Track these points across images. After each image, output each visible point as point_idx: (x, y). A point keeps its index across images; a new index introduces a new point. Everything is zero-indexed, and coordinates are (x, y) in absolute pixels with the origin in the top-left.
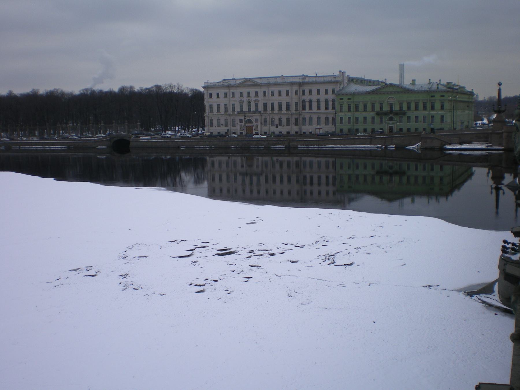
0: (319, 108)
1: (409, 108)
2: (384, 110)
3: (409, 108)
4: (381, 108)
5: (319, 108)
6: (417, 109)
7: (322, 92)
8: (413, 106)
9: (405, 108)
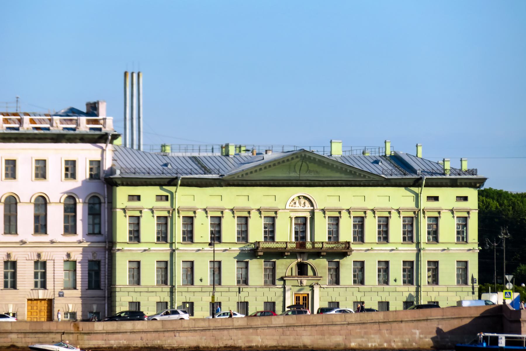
0: (41, 225)
5: (41, 225)
7: (25, 170)
9: (346, 233)
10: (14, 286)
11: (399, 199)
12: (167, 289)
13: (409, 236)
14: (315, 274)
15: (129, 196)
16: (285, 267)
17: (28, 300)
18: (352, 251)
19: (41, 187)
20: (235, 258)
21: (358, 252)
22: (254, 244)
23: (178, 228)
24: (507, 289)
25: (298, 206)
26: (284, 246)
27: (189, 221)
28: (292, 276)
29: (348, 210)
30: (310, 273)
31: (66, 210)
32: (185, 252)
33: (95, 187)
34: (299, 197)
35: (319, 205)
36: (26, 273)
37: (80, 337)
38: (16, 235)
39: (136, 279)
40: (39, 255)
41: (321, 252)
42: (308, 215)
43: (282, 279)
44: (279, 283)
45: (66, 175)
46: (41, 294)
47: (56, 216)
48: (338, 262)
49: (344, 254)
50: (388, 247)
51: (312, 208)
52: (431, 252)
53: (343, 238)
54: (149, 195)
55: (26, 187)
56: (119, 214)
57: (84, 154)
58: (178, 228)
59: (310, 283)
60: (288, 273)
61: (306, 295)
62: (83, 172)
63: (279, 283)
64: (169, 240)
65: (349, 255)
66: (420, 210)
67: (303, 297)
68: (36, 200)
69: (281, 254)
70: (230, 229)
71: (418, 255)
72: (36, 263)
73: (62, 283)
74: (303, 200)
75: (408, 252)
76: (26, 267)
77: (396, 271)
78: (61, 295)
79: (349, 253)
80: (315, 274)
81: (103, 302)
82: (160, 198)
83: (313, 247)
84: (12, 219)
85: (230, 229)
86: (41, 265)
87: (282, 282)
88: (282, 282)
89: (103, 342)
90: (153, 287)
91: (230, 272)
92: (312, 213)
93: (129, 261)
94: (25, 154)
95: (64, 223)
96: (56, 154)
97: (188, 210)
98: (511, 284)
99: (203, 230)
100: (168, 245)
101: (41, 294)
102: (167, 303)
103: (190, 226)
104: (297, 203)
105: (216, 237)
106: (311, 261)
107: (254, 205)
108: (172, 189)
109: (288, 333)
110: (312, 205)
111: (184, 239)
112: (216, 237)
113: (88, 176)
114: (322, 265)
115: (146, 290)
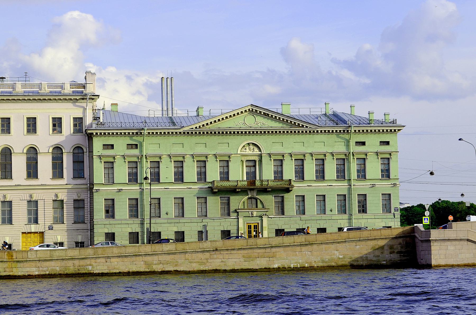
0: (32, 172)
1: (300, 174)
2: (232, 177)
3: (300, 174)
4: (225, 176)
5: (32, 172)
6: (321, 175)
7: (44, 125)
8: (310, 169)
9: (289, 172)
10: (10, 222)
11: (334, 145)
12: (138, 221)
13: (342, 174)
14: (263, 207)
15: (104, 145)
16: (237, 201)
17: (23, 233)
18: (293, 186)
19: (32, 140)
20: (195, 196)
21: (299, 188)
22: (211, 183)
23: (354, 167)
24: (425, 216)
25: (248, 152)
26: (236, 184)
27: (156, 165)
28: (244, 209)
29: (332, 153)
30: (260, 206)
31: (53, 159)
32: (360, 187)
33: (80, 140)
34: (248, 144)
35: (264, 151)
36: (20, 212)
37: (14, 265)
38: (11, 180)
39: (226, 212)
40: (31, 196)
41: (236, 189)
42: (257, 158)
43: (236, 211)
44: (234, 215)
45: (54, 130)
46: (33, 228)
47: (45, 164)
48: (283, 197)
49: (288, 190)
50: (389, 182)
51: (260, 153)
52: (360, 187)
53: (286, 177)
54: (121, 145)
55: (18, 140)
56: (96, 161)
57: (68, 113)
58: (354, 167)
59: (259, 214)
60: (241, 206)
61: (257, 224)
62: (68, 127)
63: (234, 215)
64: (346, 178)
65: (292, 190)
66: (350, 153)
67: (254, 226)
68: (28, 150)
69: (234, 191)
70: (191, 172)
71: (350, 190)
72: (29, 202)
73: (52, 218)
74: (252, 147)
75: (342, 187)
76: (20, 206)
77: (332, 203)
78: (51, 228)
79: (290, 189)
80: (263, 207)
81: (87, 234)
82: (131, 146)
83: (262, 185)
84: (8, 166)
85: (191, 172)
86: (33, 205)
87: (236, 214)
88: (236, 214)
89: (34, 269)
90: (126, 219)
91: (192, 206)
92: (261, 156)
93: (197, 198)
94: (18, 113)
95: (53, 169)
96: (44, 113)
97: (155, 156)
98: (428, 212)
99: (167, 172)
100: (346, 181)
101: (33, 228)
102: (138, 233)
103: (387, 166)
104: (247, 148)
105: (179, 177)
106: (261, 197)
107: (187, 151)
108: (139, 139)
109: (215, 256)
110: (260, 151)
111: (358, 176)
112: (179, 177)
113: (72, 131)
114: (269, 200)
115: (189, 221)
